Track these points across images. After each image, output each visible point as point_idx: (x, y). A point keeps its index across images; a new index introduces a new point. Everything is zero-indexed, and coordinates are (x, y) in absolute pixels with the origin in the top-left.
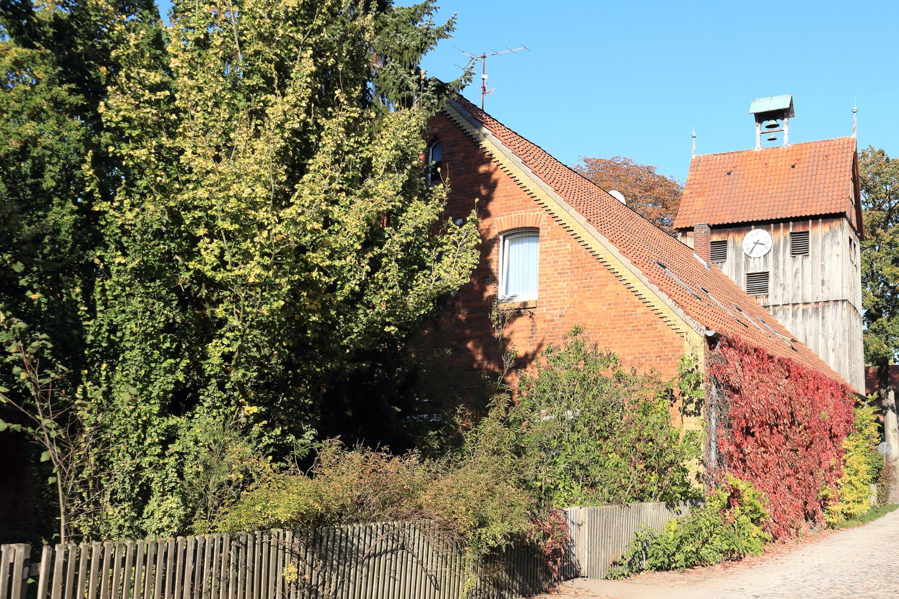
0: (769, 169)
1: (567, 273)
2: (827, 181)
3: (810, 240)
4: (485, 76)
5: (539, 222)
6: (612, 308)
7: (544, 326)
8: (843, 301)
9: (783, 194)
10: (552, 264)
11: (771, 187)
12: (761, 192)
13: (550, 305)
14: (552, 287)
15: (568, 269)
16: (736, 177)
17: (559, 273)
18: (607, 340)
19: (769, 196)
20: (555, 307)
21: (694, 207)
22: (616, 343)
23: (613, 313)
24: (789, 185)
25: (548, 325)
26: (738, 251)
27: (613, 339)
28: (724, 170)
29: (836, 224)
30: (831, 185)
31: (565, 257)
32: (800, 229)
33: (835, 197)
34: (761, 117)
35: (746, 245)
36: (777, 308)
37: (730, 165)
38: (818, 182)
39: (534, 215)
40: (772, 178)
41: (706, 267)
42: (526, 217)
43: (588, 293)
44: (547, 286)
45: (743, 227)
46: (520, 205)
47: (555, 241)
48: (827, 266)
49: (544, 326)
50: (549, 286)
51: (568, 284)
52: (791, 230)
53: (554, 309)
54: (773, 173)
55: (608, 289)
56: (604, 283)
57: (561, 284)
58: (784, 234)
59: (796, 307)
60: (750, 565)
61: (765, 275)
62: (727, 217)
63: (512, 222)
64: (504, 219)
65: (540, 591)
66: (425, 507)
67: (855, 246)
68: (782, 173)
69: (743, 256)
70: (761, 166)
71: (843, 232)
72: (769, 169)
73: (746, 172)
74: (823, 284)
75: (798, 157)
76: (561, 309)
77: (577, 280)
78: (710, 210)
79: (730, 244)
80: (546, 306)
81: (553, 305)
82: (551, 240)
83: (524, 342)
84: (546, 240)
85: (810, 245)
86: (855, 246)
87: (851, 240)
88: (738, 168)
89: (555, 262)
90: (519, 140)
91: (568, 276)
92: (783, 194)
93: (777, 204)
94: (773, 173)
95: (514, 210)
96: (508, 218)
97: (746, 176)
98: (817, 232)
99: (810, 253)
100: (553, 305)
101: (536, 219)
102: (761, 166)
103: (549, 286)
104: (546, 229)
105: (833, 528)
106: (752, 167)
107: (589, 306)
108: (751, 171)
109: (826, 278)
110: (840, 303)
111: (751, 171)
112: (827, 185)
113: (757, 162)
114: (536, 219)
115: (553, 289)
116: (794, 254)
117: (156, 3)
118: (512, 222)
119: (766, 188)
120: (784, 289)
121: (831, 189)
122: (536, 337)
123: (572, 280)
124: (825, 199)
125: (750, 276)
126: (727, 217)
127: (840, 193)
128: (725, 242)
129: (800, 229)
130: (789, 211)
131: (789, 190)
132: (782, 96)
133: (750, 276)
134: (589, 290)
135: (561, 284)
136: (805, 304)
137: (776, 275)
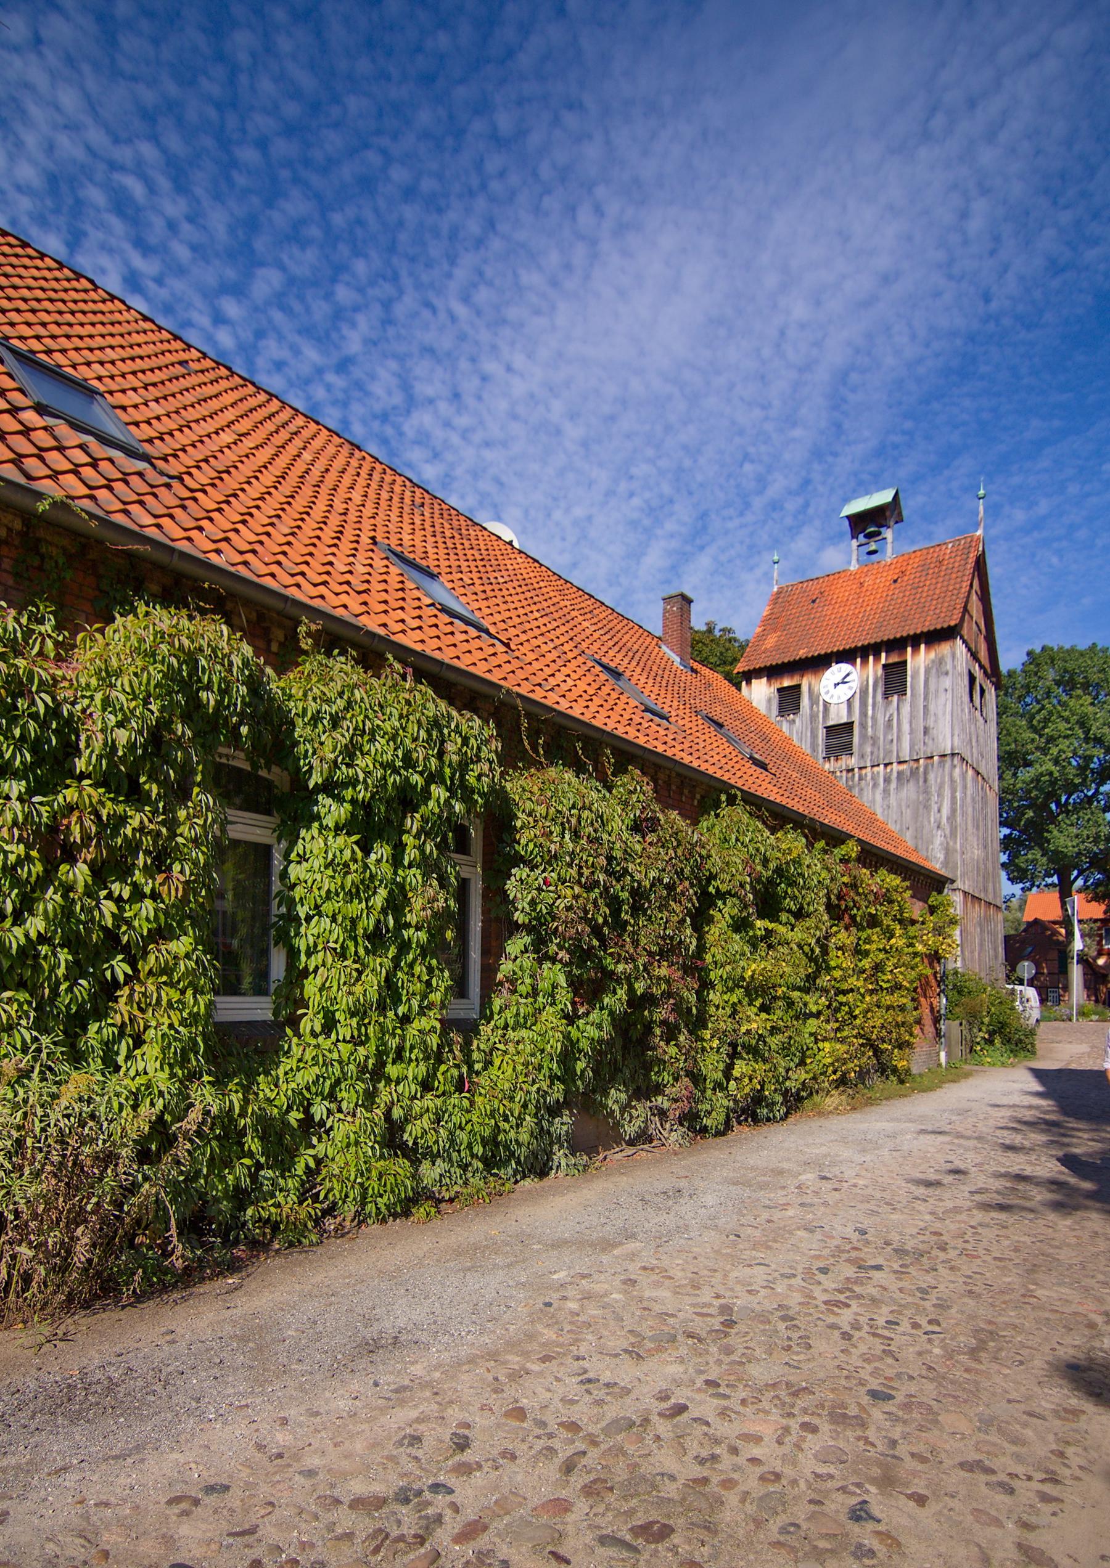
3: (909, 673)
8: (953, 755)
26: (814, 699)
29: (945, 648)
32: (894, 658)
45: (819, 663)
48: (932, 707)
52: (883, 661)
58: (873, 670)
59: (889, 769)
66: (1038, 1363)
67: (982, 691)
74: (925, 733)
79: (805, 689)
86: (982, 691)
87: (972, 679)
98: (918, 661)
105: (902, 1082)
109: (931, 723)
110: (948, 759)
116: (886, 695)
117: (1094, 1220)
120: (873, 745)
125: (830, 729)
128: (798, 687)
129: (894, 658)
133: (830, 729)
136: (900, 763)
137: (863, 726)
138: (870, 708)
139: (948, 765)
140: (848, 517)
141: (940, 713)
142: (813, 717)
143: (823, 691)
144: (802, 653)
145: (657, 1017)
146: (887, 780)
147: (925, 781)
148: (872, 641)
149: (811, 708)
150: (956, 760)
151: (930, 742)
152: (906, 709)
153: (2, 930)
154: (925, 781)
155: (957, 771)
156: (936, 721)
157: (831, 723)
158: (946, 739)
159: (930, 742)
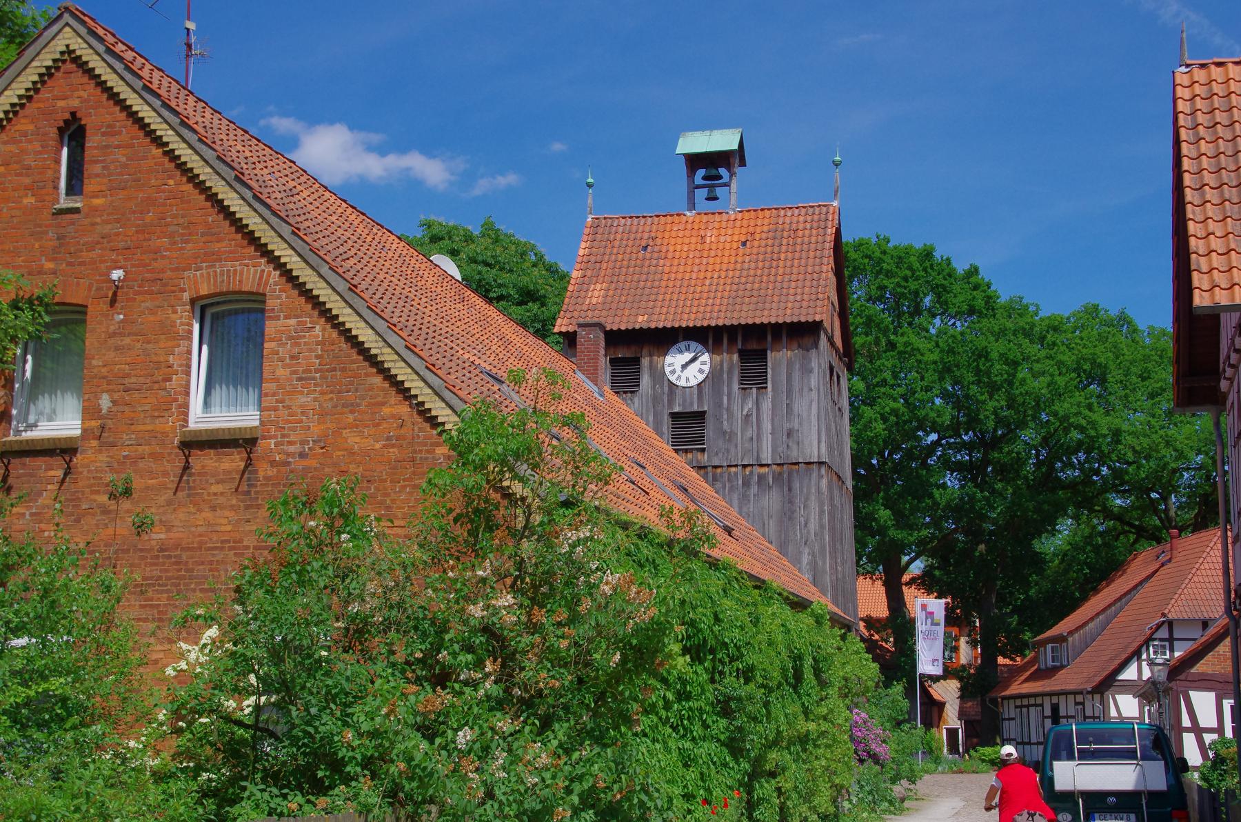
0: (707, 247)
1: (314, 379)
2: (795, 270)
4: (191, 25)
5: (265, 287)
6: (393, 446)
7: (271, 472)
9: (728, 288)
10: (288, 361)
11: (709, 275)
12: (693, 283)
13: (283, 436)
14: (287, 403)
15: (317, 371)
16: (655, 255)
17: (300, 379)
18: (382, 502)
19: (706, 289)
20: (292, 439)
21: (588, 301)
22: (399, 508)
23: (394, 453)
24: (737, 273)
25: (279, 471)
27: (393, 501)
28: (638, 242)
30: (801, 277)
31: (311, 350)
33: (806, 297)
34: (695, 161)
35: (669, 365)
36: (719, 470)
37: (646, 236)
38: (781, 271)
39: (255, 272)
40: (711, 261)
41: (596, 395)
42: (242, 273)
43: (351, 417)
44: (277, 401)
46: (231, 252)
47: (293, 322)
48: (796, 407)
49: (271, 472)
50: (282, 401)
51: (315, 399)
53: (290, 443)
54: (713, 253)
55: (386, 410)
56: (379, 399)
57: (303, 400)
60: (905, 815)
61: (700, 415)
62: (640, 319)
63: (215, 281)
64: (202, 275)
65: (898, 805)
67: (838, 377)
68: (727, 253)
69: (666, 383)
70: (693, 240)
71: (822, 356)
72: (707, 247)
73: (671, 248)
75: (751, 229)
76: (303, 443)
77: (332, 392)
78: (614, 306)
80: (275, 437)
81: (288, 436)
82: (286, 318)
83: (234, 502)
84: (278, 318)
85: (769, 370)
86: (838, 377)
87: (831, 369)
88: (658, 242)
89: (293, 358)
90: (303, 179)
91: (316, 385)
92: (728, 288)
93: (694, 276)
94: (713, 253)
95: (220, 260)
96: (209, 274)
97: (670, 256)
99: (769, 385)
100: (288, 436)
101: (261, 277)
102: (693, 240)
103: (282, 401)
104: (279, 297)
106: (680, 241)
107: (353, 440)
108: (678, 248)
111: (678, 248)
112: (794, 277)
113: (687, 233)
114: (261, 277)
115: (289, 407)
118: (215, 281)
119: (702, 275)
121: (800, 284)
122: (256, 493)
123: (322, 393)
124: (791, 298)
126: (640, 319)
127: (814, 290)
129: (753, 345)
130: (736, 315)
131: (737, 280)
132: (727, 131)
133: (674, 416)
134: (352, 412)
135: (303, 400)
137: (718, 419)
138: (725, 399)
139: (815, 475)
140: (685, 155)
141: (805, 415)
142: (656, 399)
143: (668, 370)
144: (641, 321)
145: (318, 327)
146: (746, 483)
147: (790, 490)
148: (728, 323)
149: (654, 388)
150: (823, 471)
151: (794, 447)
152: (767, 405)
153: (55, 821)
154: (790, 490)
155: (824, 482)
156: (800, 424)
157: (677, 409)
158: (813, 446)
159: (794, 447)
